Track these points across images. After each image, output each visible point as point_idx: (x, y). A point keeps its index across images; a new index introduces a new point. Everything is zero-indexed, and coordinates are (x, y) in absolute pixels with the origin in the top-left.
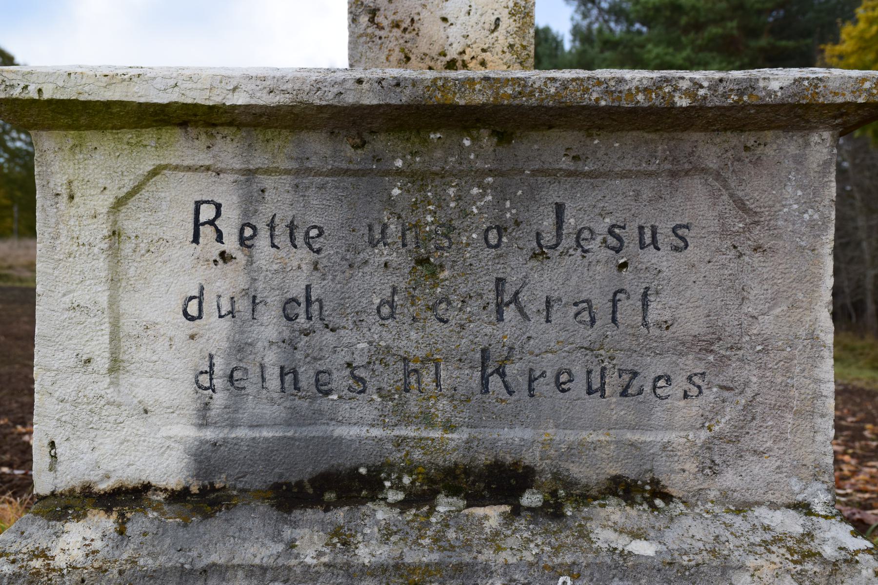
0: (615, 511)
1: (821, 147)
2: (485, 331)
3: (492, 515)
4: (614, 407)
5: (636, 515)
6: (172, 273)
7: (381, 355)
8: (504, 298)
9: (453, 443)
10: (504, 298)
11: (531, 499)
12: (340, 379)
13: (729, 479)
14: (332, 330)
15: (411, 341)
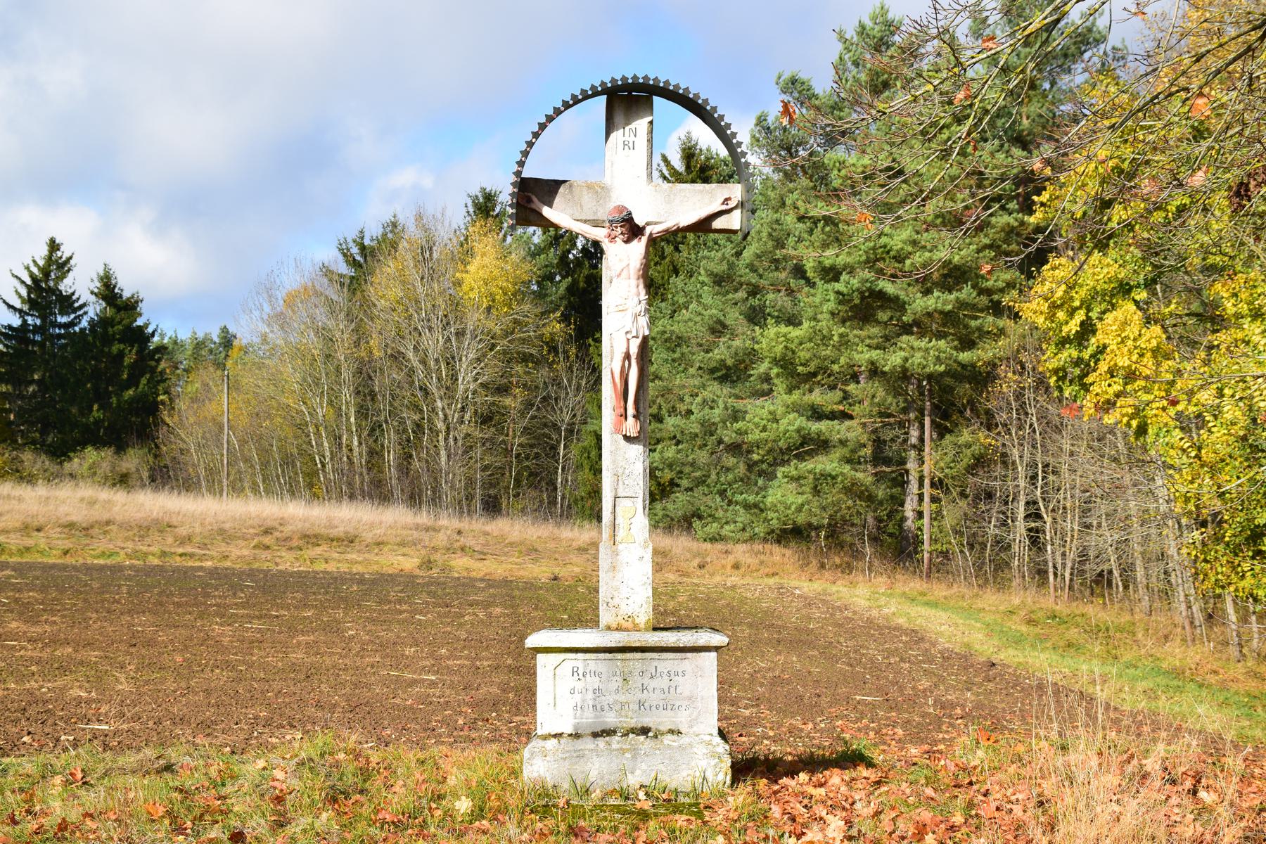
0: (670, 736)
1: (714, 654)
2: (640, 696)
3: (642, 738)
4: (669, 713)
5: (675, 737)
6: (567, 681)
7: (616, 702)
8: (644, 688)
9: (633, 722)
10: (644, 688)
11: (650, 734)
12: (606, 708)
13: (695, 729)
14: (38, 530)
15: (623, 698)
